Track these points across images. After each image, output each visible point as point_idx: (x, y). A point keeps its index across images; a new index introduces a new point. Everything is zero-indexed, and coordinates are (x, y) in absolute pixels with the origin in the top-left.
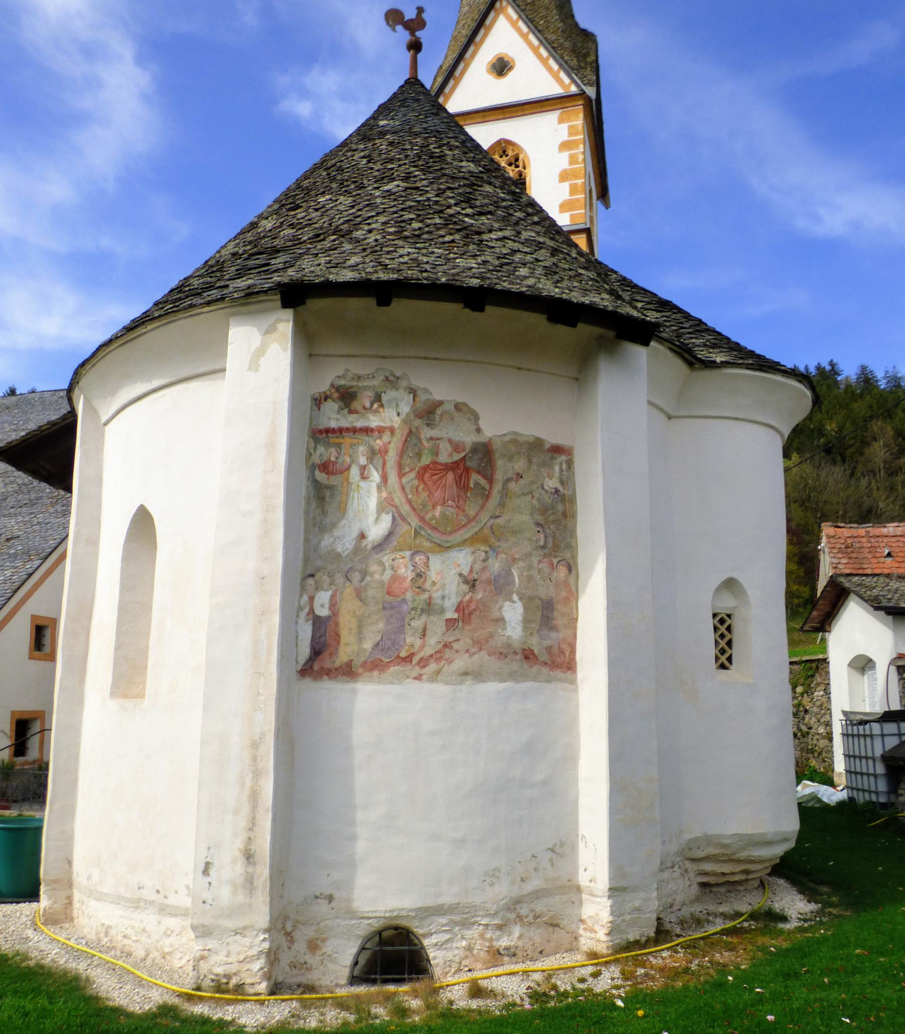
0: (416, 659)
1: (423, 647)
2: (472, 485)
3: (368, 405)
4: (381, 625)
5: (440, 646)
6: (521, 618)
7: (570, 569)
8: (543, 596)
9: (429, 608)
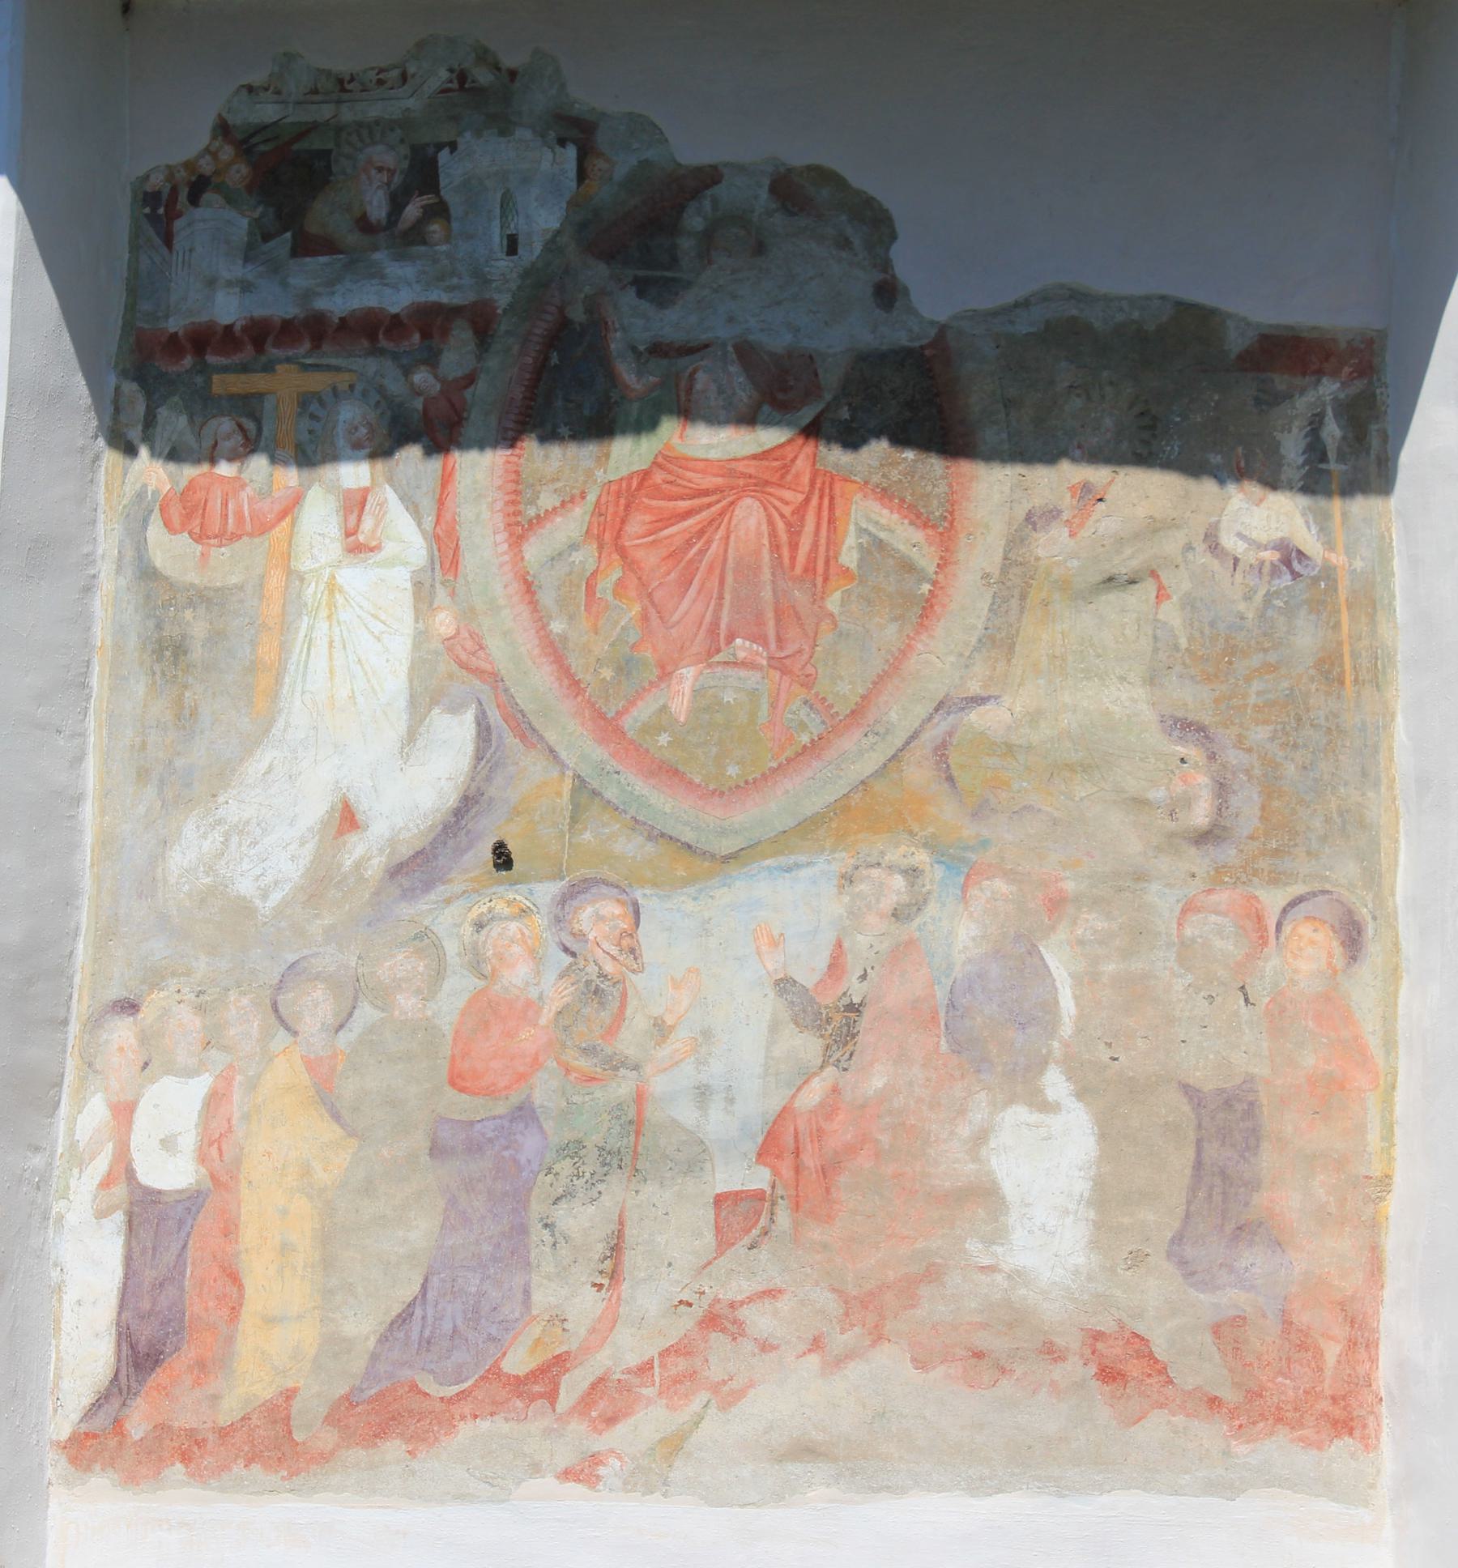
0: (572, 1386)
1: (608, 1323)
2: (849, 557)
3: (377, 206)
4: (421, 1230)
5: (686, 1322)
6: (1083, 1187)
7: (1352, 937)
8: (1202, 1075)
9: (632, 1146)
